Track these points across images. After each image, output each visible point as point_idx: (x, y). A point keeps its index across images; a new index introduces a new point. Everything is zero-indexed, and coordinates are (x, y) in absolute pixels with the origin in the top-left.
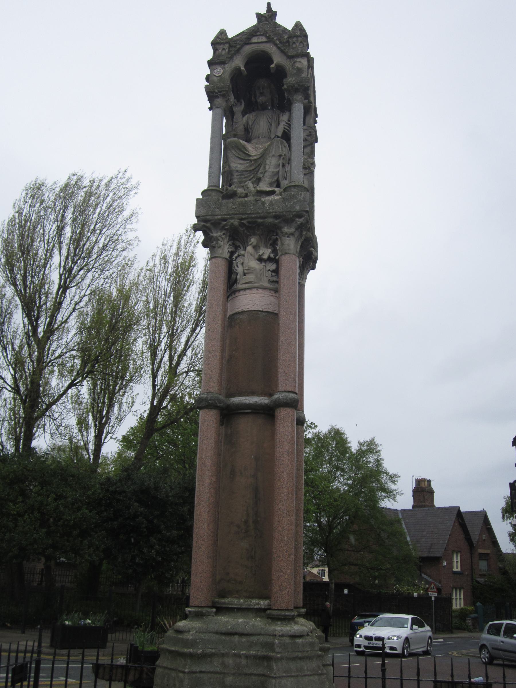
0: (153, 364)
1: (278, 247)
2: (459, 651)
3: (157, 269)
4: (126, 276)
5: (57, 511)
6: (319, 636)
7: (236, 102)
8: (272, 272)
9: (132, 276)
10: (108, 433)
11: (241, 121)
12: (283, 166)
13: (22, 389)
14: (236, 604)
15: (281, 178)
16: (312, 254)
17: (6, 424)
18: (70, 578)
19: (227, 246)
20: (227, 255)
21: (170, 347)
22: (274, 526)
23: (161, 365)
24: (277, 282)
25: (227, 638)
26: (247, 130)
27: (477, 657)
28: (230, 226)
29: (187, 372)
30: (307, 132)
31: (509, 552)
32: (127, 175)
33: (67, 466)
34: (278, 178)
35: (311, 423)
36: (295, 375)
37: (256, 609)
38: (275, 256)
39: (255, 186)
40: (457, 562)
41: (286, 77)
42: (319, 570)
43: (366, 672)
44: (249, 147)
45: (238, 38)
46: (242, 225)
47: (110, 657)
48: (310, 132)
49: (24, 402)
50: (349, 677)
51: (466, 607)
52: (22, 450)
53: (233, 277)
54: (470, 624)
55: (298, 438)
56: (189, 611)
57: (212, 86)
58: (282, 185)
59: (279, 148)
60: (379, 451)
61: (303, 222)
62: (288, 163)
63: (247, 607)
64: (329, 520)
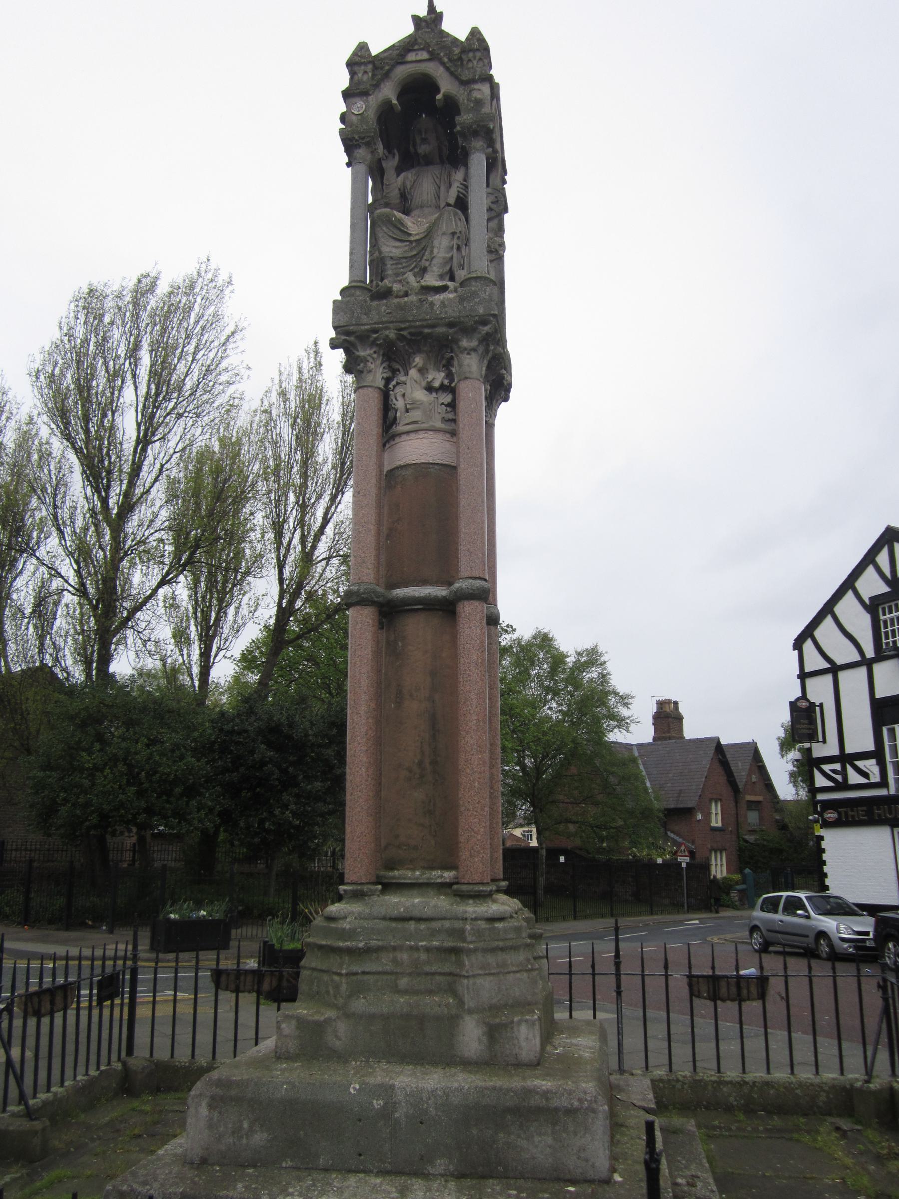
0: (278, 549)
1: (454, 370)
2: (721, 936)
3: (274, 412)
4: (232, 423)
5: (151, 761)
6: (527, 918)
7: (387, 155)
8: (446, 405)
9: (242, 420)
10: (219, 649)
11: (395, 182)
12: (459, 248)
13: (91, 590)
14: (410, 878)
15: (455, 268)
16: (504, 378)
17: (70, 640)
18: (174, 855)
19: (381, 369)
20: (380, 383)
21: (301, 523)
22: (460, 767)
23: (289, 549)
24: (454, 421)
25: (399, 925)
26: (404, 196)
27: (747, 943)
28: (384, 340)
29: (328, 559)
30: (492, 198)
31: (790, 797)
32: (213, 265)
33: (163, 698)
34: (451, 267)
35: (508, 626)
36: (483, 554)
37: (440, 883)
38: (451, 383)
39: (418, 279)
40: (716, 814)
41: (459, 113)
42: (524, 832)
43: (593, 966)
44: (408, 221)
45: (385, 55)
46: (401, 338)
47: (235, 961)
48: (496, 197)
49: (95, 608)
50: (571, 974)
51: (730, 876)
52: (96, 677)
53: (391, 414)
54: (737, 898)
55: (490, 644)
56: (345, 891)
57: (349, 129)
58: (457, 278)
59: (452, 222)
60: (605, 663)
61: (490, 331)
62: (466, 245)
63: (425, 881)
64: (536, 761)
